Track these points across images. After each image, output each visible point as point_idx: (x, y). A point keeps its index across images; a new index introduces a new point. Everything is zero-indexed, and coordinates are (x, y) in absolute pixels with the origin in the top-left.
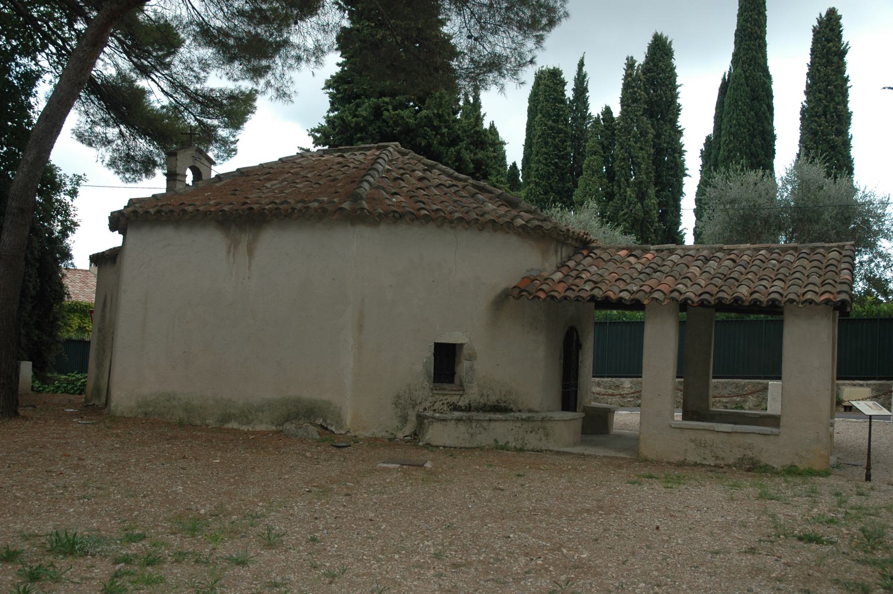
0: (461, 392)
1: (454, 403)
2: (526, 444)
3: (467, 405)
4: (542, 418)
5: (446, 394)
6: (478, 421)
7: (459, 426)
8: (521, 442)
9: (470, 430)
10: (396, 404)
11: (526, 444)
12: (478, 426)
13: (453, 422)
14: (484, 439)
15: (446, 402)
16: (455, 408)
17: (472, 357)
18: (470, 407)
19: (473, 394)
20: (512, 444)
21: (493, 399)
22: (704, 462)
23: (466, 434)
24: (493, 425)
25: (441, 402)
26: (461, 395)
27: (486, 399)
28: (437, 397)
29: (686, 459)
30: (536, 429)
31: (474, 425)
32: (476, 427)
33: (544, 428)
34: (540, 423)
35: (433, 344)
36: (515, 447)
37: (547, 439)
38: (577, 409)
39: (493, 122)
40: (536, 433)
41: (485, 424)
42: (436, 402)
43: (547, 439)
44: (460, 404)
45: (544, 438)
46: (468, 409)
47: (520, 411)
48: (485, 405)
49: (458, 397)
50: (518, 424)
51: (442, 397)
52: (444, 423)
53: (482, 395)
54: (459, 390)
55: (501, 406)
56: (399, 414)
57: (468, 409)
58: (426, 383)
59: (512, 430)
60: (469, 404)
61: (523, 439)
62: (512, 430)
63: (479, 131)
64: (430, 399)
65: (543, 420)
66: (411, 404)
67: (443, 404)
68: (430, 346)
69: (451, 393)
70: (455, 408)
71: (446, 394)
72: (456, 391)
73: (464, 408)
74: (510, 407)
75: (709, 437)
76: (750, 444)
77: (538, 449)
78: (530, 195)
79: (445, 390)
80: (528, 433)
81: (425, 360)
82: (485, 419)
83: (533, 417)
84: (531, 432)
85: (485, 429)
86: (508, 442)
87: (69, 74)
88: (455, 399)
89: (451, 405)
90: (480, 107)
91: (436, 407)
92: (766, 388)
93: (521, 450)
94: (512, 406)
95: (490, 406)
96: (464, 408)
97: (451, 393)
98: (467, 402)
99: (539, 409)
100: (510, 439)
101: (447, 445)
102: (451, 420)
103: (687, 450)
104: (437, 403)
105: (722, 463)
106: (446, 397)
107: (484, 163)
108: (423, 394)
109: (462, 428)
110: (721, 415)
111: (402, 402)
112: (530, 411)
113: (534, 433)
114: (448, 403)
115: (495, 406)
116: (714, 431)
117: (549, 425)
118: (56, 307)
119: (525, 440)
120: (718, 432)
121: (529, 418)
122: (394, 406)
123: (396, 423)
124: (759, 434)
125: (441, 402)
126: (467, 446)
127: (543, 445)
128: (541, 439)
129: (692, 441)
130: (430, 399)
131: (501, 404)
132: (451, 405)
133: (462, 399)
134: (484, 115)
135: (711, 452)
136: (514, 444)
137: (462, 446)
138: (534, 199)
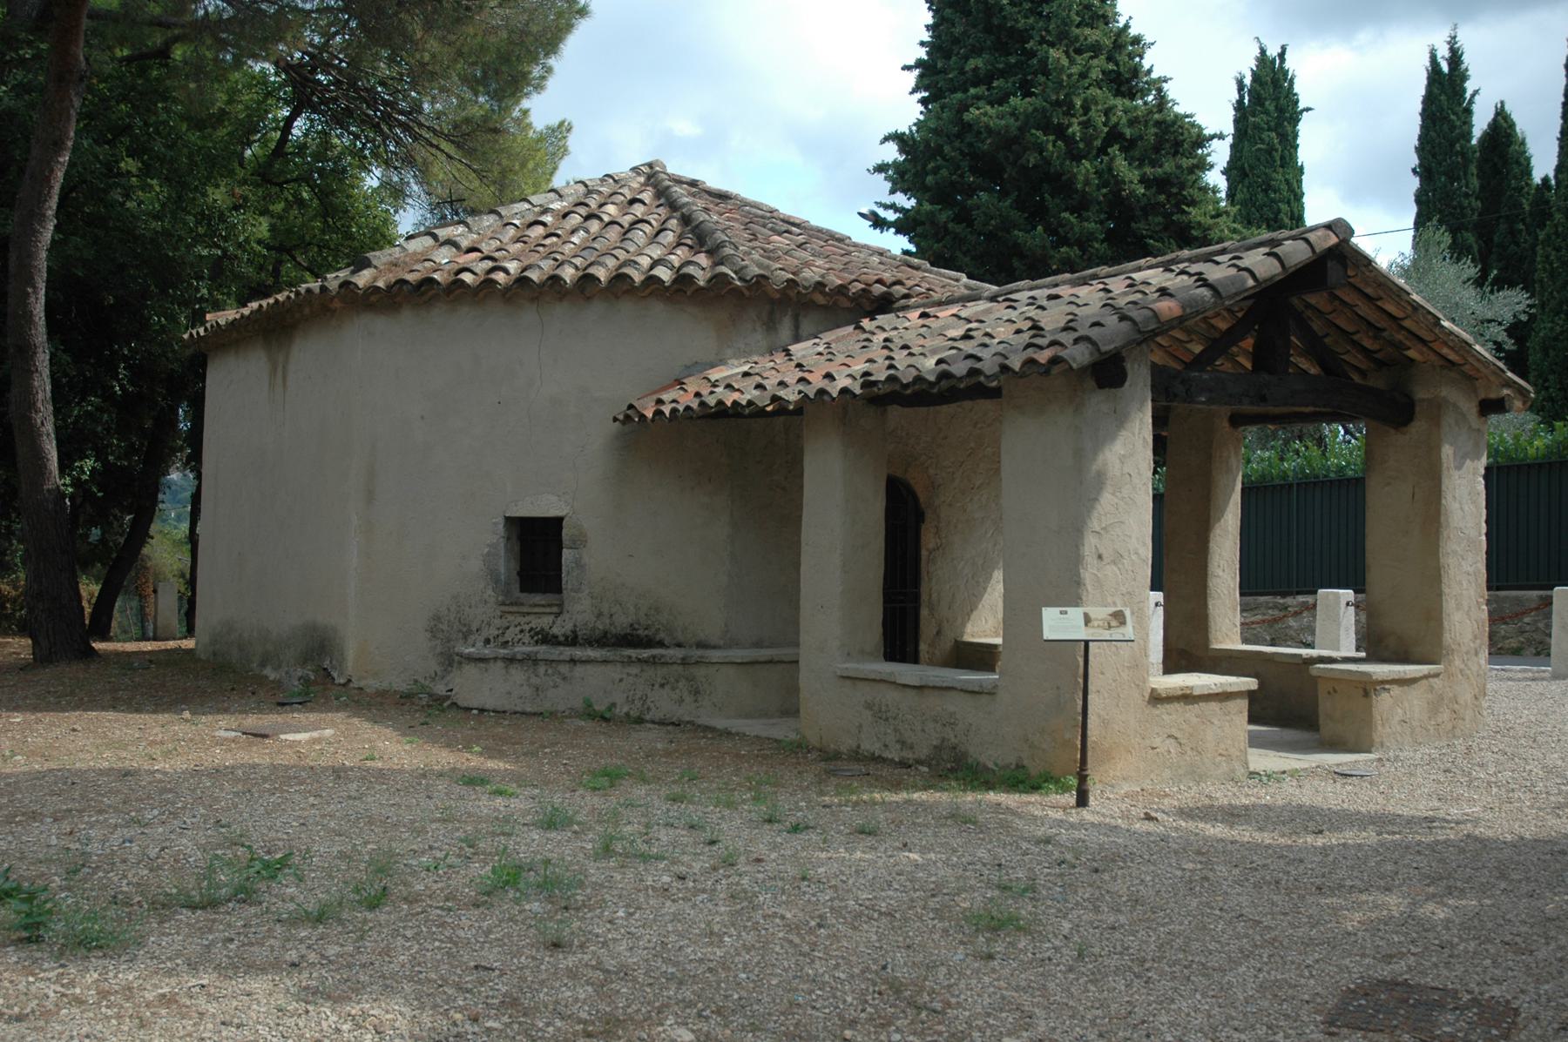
0: (555, 609)
1: (542, 629)
2: (649, 709)
3: (569, 633)
4: (683, 659)
5: (528, 614)
6: (551, 662)
7: (513, 671)
8: (638, 704)
9: (534, 680)
10: (433, 632)
11: (649, 709)
12: (550, 671)
13: (500, 664)
14: (561, 696)
15: (527, 628)
16: (547, 639)
17: (580, 542)
18: (576, 637)
19: (579, 610)
20: (622, 710)
21: (622, 622)
22: (887, 755)
23: (525, 687)
24: (579, 670)
25: (519, 628)
26: (558, 615)
27: (608, 621)
28: (510, 618)
29: (859, 747)
30: (672, 680)
31: (542, 669)
32: (546, 674)
33: (691, 679)
34: (680, 668)
35: (501, 521)
36: (627, 714)
37: (696, 701)
38: (923, 647)
39: (1502, 103)
40: (673, 689)
41: (564, 669)
42: (508, 628)
43: (696, 701)
44: (555, 630)
45: (688, 699)
46: (572, 640)
47: (679, 645)
48: (606, 633)
49: (551, 618)
50: (634, 670)
51: (520, 619)
52: (482, 665)
53: (600, 615)
54: (550, 606)
55: (638, 636)
56: (439, 650)
57: (572, 640)
58: (490, 592)
59: (621, 680)
60: (574, 632)
61: (644, 699)
62: (621, 680)
63: (1164, 122)
64: (497, 622)
65: (684, 662)
66: (460, 631)
67: (522, 631)
68: (495, 524)
69: (536, 610)
70: (547, 639)
71: (528, 614)
72: (543, 606)
73: (562, 639)
74: (658, 638)
75: (890, 696)
76: (952, 714)
77: (674, 720)
78: (1553, 237)
79: (522, 604)
80: (657, 686)
81: (486, 550)
82: (561, 658)
83: (663, 656)
84: (662, 686)
85: (564, 679)
86: (614, 705)
87: (84, 99)
88: (544, 622)
89: (537, 634)
90: (1464, 77)
91: (508, 636)
92: (1548, 602)
93: (640, 721)
94: (662, 635)
95: (615, 636)
96: (562, 639)
97: (536, 610)
98: (569, 627)
99: (722, 643)
100: (619, 698)
101: (487, 707)
102: (495, 659)
103: (861, 726)
104: (511, 629)
105: (910, 756)
106: (527, 619)
107: (1176, 181)
108: (484, 613)
109: (518, 674)
110: (1230, 657)
111: (445, 627)
112: (701, 645)
113: (667, 688)
114: (531, 629)
115: (626, 635)
116: (894, 683)
117: (700, 672)
118: (163, 480)
119: (648, 702)
120: (905, 686)
121: (654, 657)
122: (428, 635)
123: (434, 666)
124: (962, 690)
125: (519, 628)
126: (529, 709)
127: (684, 712)
128: (681, 701)
129: (869, 706)
130: (497, 622)
131: (640, 632)
132: (537, 634)
133: (559, 621)
134: (1476, 92)
135: (896, 730)
136: (625, 709)
137: (518, 709)
138: (1563, 244)
